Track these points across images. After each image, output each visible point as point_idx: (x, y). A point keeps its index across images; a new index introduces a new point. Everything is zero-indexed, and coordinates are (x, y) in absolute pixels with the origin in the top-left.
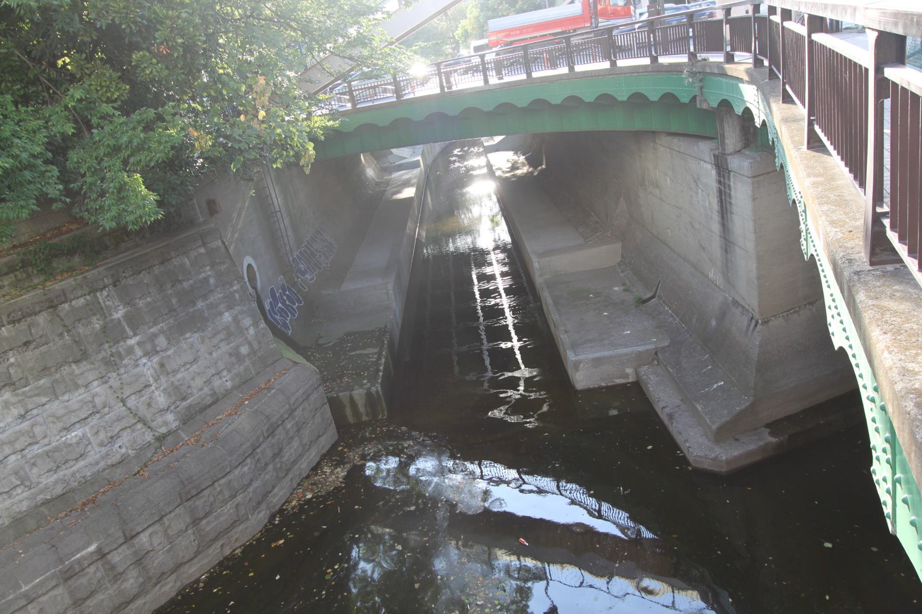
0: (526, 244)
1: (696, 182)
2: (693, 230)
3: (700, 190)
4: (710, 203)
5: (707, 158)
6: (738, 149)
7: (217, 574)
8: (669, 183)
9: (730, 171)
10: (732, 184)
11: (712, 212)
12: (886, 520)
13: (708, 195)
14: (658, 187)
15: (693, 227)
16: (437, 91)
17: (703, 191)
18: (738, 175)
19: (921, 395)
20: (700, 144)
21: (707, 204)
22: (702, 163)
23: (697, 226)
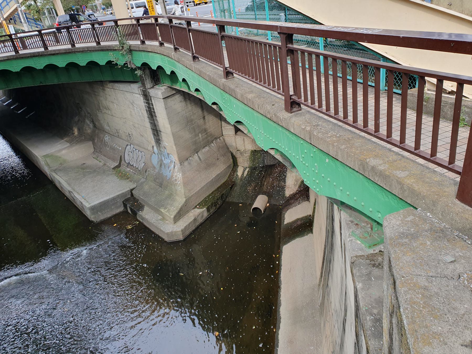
0: (33, 151)
1: (132, 104)
2: (134, 128)
3: (135, 108)
4: (142, 113)
5: (137, 92)
6: (152, 86)
7: (211, 272)
8: (116, 107)
9: (151, 97)
10: (153, 102)
11: (144, 118)
12: (448, 170)
13: (141, 110)
14: (109, 109)
15: (135, 127)
16: (464, 94)
17: (137, 108)
18: (155, 98)
19: (93, 353)
20: (131, 85)
21: (141, 115)
22: (134, 94)
23: (136, 126)
